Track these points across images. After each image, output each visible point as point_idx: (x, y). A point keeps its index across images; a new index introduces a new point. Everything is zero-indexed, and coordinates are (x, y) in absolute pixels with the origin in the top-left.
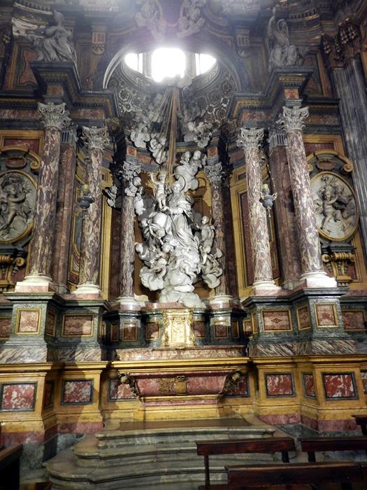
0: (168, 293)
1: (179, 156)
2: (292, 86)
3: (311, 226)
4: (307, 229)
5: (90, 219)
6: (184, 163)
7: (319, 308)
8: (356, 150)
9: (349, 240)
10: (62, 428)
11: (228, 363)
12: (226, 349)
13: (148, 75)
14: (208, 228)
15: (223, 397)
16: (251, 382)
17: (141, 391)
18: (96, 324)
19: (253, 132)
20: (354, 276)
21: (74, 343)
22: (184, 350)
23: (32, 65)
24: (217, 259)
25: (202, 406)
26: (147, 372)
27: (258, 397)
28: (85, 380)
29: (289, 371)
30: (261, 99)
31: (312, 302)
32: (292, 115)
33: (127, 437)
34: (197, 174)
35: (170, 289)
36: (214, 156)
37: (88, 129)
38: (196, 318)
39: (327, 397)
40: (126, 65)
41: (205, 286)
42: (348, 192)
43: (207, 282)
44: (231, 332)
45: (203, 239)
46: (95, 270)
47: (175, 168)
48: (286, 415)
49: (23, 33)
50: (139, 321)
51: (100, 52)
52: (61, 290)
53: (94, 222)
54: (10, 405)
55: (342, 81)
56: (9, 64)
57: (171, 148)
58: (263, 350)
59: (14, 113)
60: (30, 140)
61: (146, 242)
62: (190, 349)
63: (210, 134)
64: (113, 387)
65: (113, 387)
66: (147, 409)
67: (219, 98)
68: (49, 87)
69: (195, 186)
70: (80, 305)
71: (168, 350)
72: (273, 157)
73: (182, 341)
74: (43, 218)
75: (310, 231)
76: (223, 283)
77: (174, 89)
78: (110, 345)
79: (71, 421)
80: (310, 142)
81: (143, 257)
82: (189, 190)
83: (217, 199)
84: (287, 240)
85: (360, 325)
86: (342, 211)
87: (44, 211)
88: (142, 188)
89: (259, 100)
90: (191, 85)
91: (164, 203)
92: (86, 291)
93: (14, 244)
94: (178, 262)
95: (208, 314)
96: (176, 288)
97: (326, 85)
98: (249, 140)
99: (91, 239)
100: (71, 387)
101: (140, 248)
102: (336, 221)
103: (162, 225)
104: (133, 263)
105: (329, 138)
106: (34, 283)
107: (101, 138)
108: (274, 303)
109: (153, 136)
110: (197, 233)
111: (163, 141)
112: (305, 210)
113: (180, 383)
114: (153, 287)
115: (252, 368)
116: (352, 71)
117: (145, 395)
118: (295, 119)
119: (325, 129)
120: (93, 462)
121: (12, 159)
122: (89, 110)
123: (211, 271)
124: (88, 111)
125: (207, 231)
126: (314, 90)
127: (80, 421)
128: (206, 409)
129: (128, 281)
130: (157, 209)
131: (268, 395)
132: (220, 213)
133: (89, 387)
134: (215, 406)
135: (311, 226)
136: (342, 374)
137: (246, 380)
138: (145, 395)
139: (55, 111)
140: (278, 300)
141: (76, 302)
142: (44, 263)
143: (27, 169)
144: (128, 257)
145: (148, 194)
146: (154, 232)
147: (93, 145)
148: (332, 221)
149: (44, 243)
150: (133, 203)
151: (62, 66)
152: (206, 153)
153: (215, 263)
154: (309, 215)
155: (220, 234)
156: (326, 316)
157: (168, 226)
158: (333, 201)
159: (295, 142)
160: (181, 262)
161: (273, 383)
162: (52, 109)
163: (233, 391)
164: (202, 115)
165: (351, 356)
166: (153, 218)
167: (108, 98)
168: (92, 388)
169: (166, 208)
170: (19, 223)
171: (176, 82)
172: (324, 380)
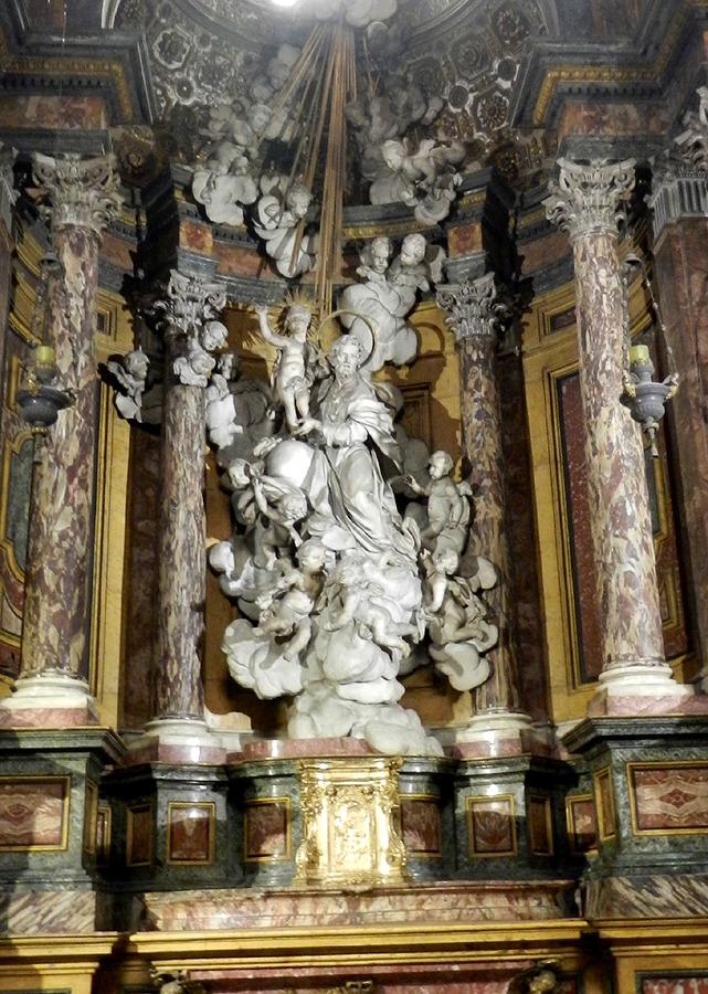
1: (354, 251)
6: (372, 275)
11: (517, 937)
12: (510, 893)
19: (600, 171)
22: (372, 894)
24: (479, 592)
30: (625, 62)
34: (412, 311)
43: (446, 669)
53: (71, 473)
57: (326, 228)
58: (631, 895)
61: (243, 536)
63: (458, 179)
69: (408, 352)
70: (25, 745)
76: (501, 675)
82: (387, 363)
83: (480, 394)
88: (229, 360)
89: (620, 65)
91: (305, 409)
94: (352, 603)
96: (343, 690)
101: (225, 557)
103: (299, 482)
107: (93, 194)
108: (668, 741)
109: (267, 185)
110: (413, 508)
124: (52, 102)
125: (446, 502)
129: (186, 665)
140: (684, 730)
144: (183, 589)
146: (272, 505)
147: (69, 217)
152: (443, 243)
155: (490, 510)
157: (318, 485)
164: (430, 115)
167: (119, 59)
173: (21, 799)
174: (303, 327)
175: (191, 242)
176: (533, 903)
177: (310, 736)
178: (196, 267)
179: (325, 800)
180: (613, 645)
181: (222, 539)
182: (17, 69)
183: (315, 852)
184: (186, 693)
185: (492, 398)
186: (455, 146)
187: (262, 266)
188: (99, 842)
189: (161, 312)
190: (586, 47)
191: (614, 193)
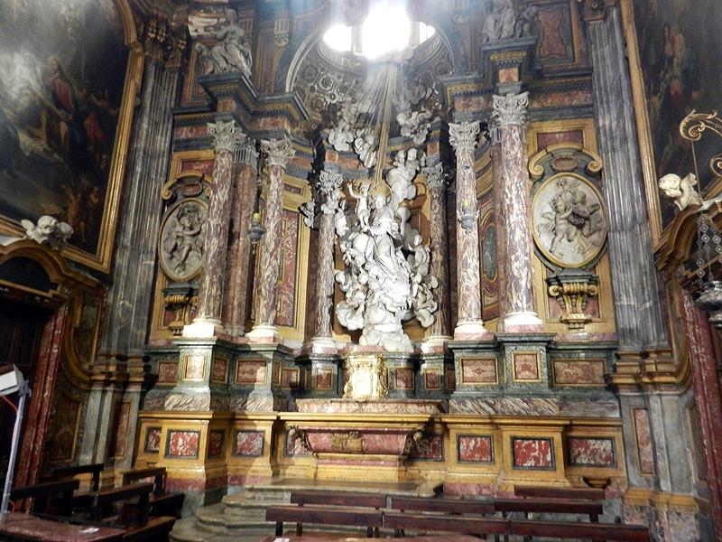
1: (393, 155)
2: (509, 65)
3: (519, 253)
4: (513, 257)
5: (267, 249)
6: (399, 165)
7: (518, 357)
8: (612, 138)
9: (592, 265)
10: (232, 480)
11: (405, 420)
12: (418, 404)
13: (358, 51)
14: (422, 250)
15: (409, 458)
17: (313, 447)
19: (512, 99)
21: (245, 391)
22: (366, 402)
23: (200, 81)
24: (432, 290)
25: (380, 468)
26: (316, 426)
28: (255, 431)
29: (488, 433)
30: (476, 81)
32: (507, 105)
33: (275, 490)
34: (415, 178)
37: (267, 142)
39: (514, 464)
40: (325, 46)
43: (420, 319)
45: (417, 264)
46: (272, 309)
48: (479, 485)
49: (201, 32)
51: (284, 43)
52: (235, 331)
53: (271, 254)
54: (177, 452)
55: (601, 40)
56: (187, 72)
57: (381, 149)
58: (456, 407)
60: (208, 161)
61: (348, 269)
63: (429, 125)
66: (320, 466)
68: (219, 102)
69: (413, 195)
70: (252, 349)
73: (368, 393)
74: (211, 255)
75: (517, 259)
76: (439, 321)
79: (241, 473)
80: (549, 131)
81: (345, 288)
82: (405, 199)
83: (436, 211)
85: (597, 379)
87: (212, 249)
88: (344, 202)
89: (476, 83)
90: (412, 58)
91: (366, 221)
93: (190, 281)
94: (377, 295)
96: (376, 327)
97: (578, 46)
99: (267, 273)
100: (243, 437)
101: (341, 277)
102: (569, 241)
103: (362, 251)
105: (574, 124)
106: (201, 330)
107: (281, 152)
108: (476, 350)
109: (359, 133)
110: (410, 257)
111: (371, 140)
112: (513, 232)
113: (355, 441)
114: (352, 326)
116: (612, 25)
117: (317, 451)
118: (510, 110)
119: (571, 111)
120: (236, 511)
121: (189, 186)
122: (270, 118)
123: (424, 305)
124: (269, 119)
125: (421, 255)
126: (561, 55)
127: (250, 473)
129: (325, 318)
132: (432, 230)
133: (261, 438)
134: (395, 468)
136: (537, 439)
139: (224, 130)
140: (481, 346)
142: (212, 305)
144: (325, 290)
146: (353, 258)
147: (273, 162)
148: (565, 241)
149: (212, 283)
151: (230, 77)
152: (425, 150)
154: (517, 238)
155: (438, 257)
156: (526, 368)
157: (370, 251)
159: (508, 142)
160: (387, 290)
161: (468, 446)
162: (221, 129)
163: (425, 453)
164: (428, 95)
166: (352, 241)
167: (290, 102)
170: (194, 259)
171: (393, 57)
172: (513, 445)
173: (252, 367)
174: (366, 190)
175: (330, 159)
176: (428, 408)
177: (366, 344)
178: (331, 168)
179: (355, 368)
180: (462, 313)
181: (342, 270)
182: (256, 109)
183: (351, 387)
184: (325, 327)
185: (441, 212)
186: (428, 112)
187: (359, 164)
188: (637, 358)
189: (319, 186)
190: (460, 77)
191: (472, 135)
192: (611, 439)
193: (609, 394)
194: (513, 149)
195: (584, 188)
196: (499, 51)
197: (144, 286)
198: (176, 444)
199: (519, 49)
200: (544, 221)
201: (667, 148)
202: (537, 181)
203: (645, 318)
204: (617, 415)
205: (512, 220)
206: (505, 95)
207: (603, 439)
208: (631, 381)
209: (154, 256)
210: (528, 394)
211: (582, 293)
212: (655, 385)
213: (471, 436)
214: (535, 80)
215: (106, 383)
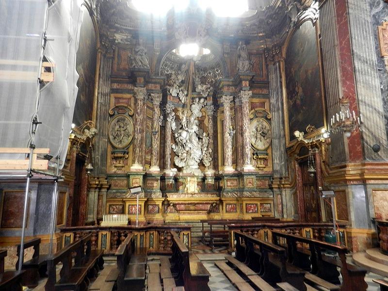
0: (187, 169)
1: (193, 99)
2: (246, 80)
4: (246, 147)
9: (266, 150)
12: (211, 194)
15: (209, 212)
16: (221, 207)
18: (159, 183)
19: (228, 97)
20: (266, 165)
22: (195, 194)
26: (180, 202)
27: (223, 213)
28: (156, 205)
31: (245, 177)
35: (187, 167)
36: (210, 102)
38: (199, 180)
41: (204, 165)
42: (268, 128)
43: (204, 163)
44: (214, 187)
47: (191, 106)
49: (120, 41)
50: (174, 181)
57: (189, 96)
59: (118, 85)
61: (176, 144)
62: (197, 194)
63: (209, 90)
64: (166, 208)
65: (166, 208)
67: (214, 68)
68: (138, 78)
70: (153, 175)
71: (188, 194)
72: (237, 110)
73: (194, 191)
74: (139, 141)
77: (192, 61)
78: (164, 190)
81: (175, 150)
84: (239, 149)
86: (264, 137)
92: (155, 169)
93: (123, 148)
94: (192, 155)
95: (204, 179)
97: (265, 72)
98: (226, 101)
99: (156, 147)
101: (174, 146)
104: (170, 154)
105: (262, 100)
108: (231, 176)
110: (200, 140)
115: (221, 202)
117: (179, 211)
119: (262, 96)
124: (153, 85)
128: (204, 216)
130: (182, 128)
131: (226, 212)
135: (248, 146)
137: (219, 206)
138: (179, 211)
141: (151, 174)
143: (127, 114)
144: (168, 152)
145: (177, 119)
148: (259, 141)
150: (171, 124)
153: (208, 155)
154: (248, 141)
155: (211, 141)
156: (250, 183)
157: (188, 137)
158: (261, 132)
162: (156, 96)
165: (257, 198)
168: (159, 208)
169: (187, 129)
170: (126, 140)
173: (152, 182)
192: (270, 204)
193: (270, 190)
194: (246, 110)
195: (265, 124)
196: (243, 75)
197: (103, 149)
198: (132, 210)
199: (249, 76)
200: (253, 134)
201: (293, 118)
202: (251, 119)
203: (281, 168)
204: (272, 196)
205: (246, 135)
206: (245, 91)
207: (267, 204)
208: (277, 186)
209: (107, 138)
210: (251, 191)
211: (264, 158)
212: (284, 188)
213: (230, 204)
214: (253, 85)
215: (96, 188)
